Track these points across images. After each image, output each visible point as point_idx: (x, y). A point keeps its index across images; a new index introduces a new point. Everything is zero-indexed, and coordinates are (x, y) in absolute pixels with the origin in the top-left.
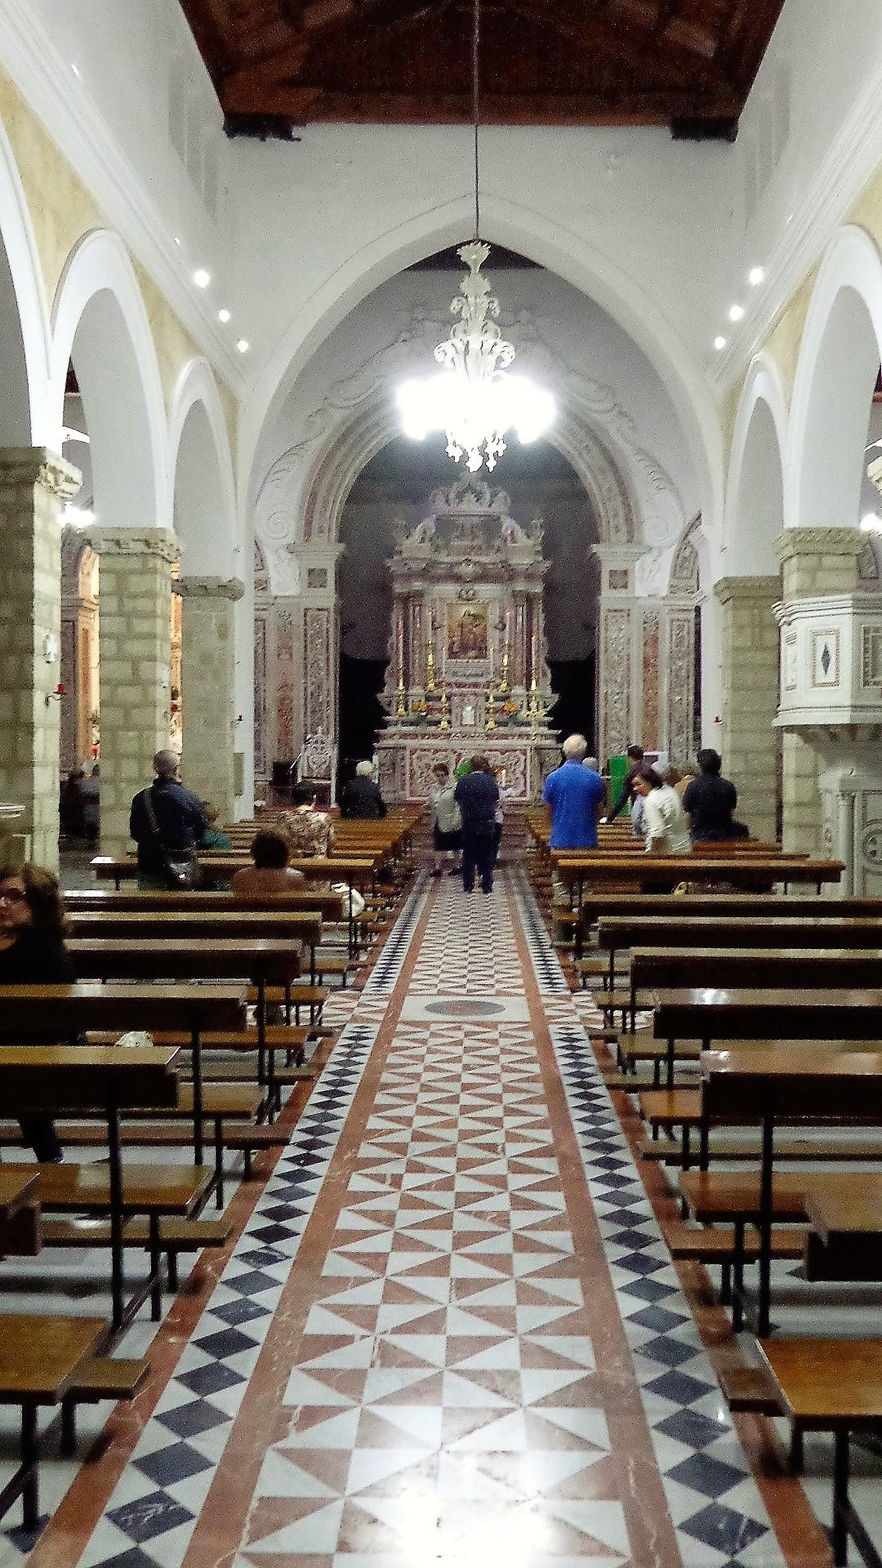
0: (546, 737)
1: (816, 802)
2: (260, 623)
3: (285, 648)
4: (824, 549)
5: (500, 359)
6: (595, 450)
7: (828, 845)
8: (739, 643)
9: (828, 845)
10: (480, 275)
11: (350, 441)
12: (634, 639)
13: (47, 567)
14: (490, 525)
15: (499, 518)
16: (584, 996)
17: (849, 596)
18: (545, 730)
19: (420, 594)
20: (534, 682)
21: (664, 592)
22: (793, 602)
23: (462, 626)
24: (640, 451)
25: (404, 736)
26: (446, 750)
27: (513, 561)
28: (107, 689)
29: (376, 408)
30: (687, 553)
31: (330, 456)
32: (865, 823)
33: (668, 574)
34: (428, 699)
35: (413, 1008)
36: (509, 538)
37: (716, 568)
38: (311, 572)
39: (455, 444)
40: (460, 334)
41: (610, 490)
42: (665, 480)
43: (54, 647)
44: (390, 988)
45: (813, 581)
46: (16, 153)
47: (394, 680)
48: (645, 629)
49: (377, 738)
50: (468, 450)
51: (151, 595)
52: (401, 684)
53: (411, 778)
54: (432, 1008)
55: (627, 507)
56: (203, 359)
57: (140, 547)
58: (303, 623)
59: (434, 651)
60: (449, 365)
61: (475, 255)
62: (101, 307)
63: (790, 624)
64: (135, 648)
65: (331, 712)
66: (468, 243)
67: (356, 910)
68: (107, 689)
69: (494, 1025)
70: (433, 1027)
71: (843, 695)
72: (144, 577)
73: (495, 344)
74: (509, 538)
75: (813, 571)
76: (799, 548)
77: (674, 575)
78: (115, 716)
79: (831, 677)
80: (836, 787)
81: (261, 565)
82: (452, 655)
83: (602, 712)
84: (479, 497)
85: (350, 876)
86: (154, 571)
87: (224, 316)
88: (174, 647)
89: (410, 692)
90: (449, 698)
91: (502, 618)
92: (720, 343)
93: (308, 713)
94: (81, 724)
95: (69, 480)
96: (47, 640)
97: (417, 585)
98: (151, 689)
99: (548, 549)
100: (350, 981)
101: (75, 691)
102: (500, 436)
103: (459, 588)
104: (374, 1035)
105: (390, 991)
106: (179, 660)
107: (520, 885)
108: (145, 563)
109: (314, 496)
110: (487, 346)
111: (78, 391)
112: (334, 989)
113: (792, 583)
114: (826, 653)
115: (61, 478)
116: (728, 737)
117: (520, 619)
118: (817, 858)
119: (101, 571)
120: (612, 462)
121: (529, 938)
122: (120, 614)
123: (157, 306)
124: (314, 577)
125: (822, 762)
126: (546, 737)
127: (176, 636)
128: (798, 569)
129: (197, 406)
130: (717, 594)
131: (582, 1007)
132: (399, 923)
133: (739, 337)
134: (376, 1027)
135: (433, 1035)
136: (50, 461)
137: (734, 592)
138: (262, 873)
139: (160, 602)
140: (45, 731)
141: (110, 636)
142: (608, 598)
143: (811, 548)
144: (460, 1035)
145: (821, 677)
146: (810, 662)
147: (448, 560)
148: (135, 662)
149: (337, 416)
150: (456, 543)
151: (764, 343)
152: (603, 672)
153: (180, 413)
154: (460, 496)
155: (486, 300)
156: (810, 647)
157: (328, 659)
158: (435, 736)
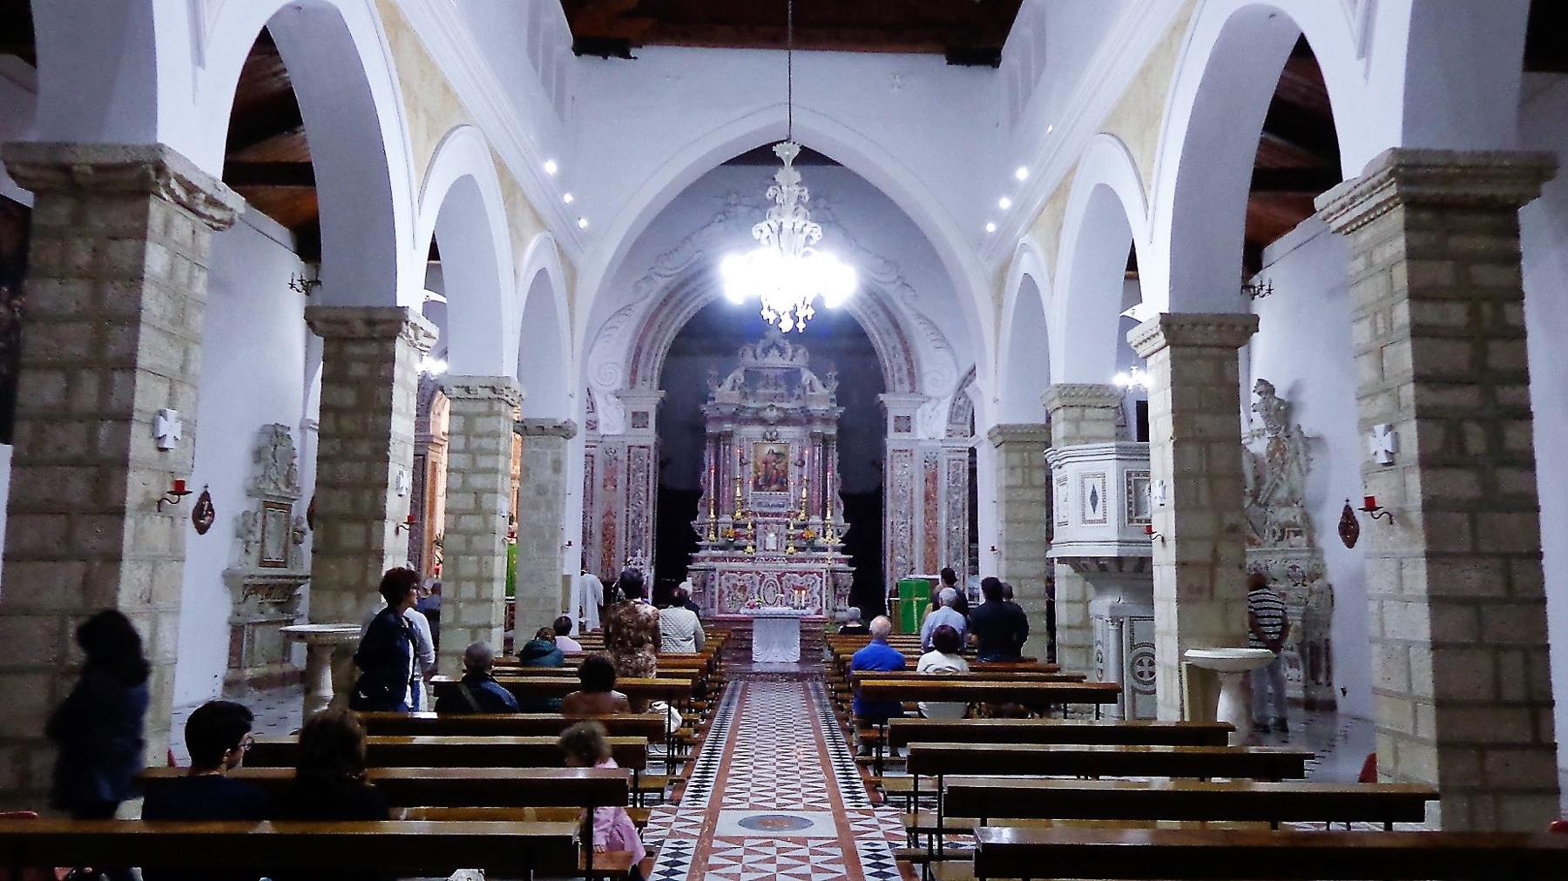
0: (840, 560)
1: (1086, 625)
2: (590, 457)
3: (610, 480)
4: (1088, 402)
5: (809, 238)
6: (882, 315)
7: (1100, 666)
8: (1012, 482)
9: (1100, 666)
10: (792, 168)
11: (671, 304)
12: (916, 475)
13: (404, 410)
14: (792, 377)
15: (799, 370)
16: (885, 810)
17: (1113, 444)
18: (838, 555)
19: (730, 435)
20: (829, 513)
21: (943, 435)
22: (1060, 447)
23: (766, 463)
24: (920, 316)
25: (714, 559)
26: (750, 572)
27: (811, 408)
28: (452, 518)
29: (700, 273)
30: (961, 402)
31: (654, 316)
32: (1133, 647)
33: (946, 420)
34: (735, 526)
35: (728, 824)
36: (808, 389)
37: (990, 417)
38: (635, 414)
39: (769, 309)
40: (774, 216)
41: (894, 348)
42: (943, 341)
43: (406, 482)
44: (704, 803)
45: (1078, 428)
46: (397, 62)
47: (706, 510)
48: (925, 467)
49: (691, 560)
50: (781, 314)
51: (495, 435)
52: (712, 513)
53: (719, 597)
54: (743, 823)
55: (909, 361)
56: (549, 235)
57: (487, 393)
58: (626, 459)
59: (742, 483)
60: (766, 242)
61: (787, 152)
62: (463, 189)
63: (1060, 467)
64: (478, 481)
65: (649, 537)
66: (782, 142)
67: (674, 726)
68: (452, 518)
69: (803, 841)
70: (747, 843)
71: (1110, 531)
72: (489, 419)
73: (806, 225)
74: (808, 389)
75: (1077, 422)
76: (1065, 401)
77: (950, 421)
78: (456, 542)
79: (1099, 515)
80: (1106, 614)
81: (592, 407)
82: (757, 487)
83: (889, 539)
84: (782, 352)
85: (668, 694)
86: (499, 414)
87: (568, 198)
88: (513, 478)
89: (721, 520)
90: (754, 526)
91: (802, 455)
92: (991, 227)
93: (630, 538)
94: (426, 546)
95: (428, 335)
96: (400, 474)
97: (728, 427)
98: (492, 518)
99: (841, 397)
100: (668, 794)
101: (422, 517)
102: (809, 301)
103: (765, 430)
104: (691, 851)
105: (705, 805)
106: (516, 489)
107: (819, 697)
108: (491, 407)
109: (639, 350)
110: (798, 227)
111: (439, 259)
112: (653, 802)
113: (1059, 430)
114: (1094, 493)
115: (421, 333)
116: (1003, 564)
117: (817, 457)
118: (1093, 680)
119: (451, 413)
120: (896, 326)
121: (830, 750)
122: (467, 450)
123: (510, 188)
124: (638, 419)
125: (1091, 590)
126: (840, 560)
127: (516, 470)
128: (1064, 420)
129: (542, 273)
130: (990, 438)
131: (886, 822)
132: (711, 736)
133: (1008, 224)
134: (693, 843)
135: (748, 851)
136: (412, 319)
137: (1008, 438)
138: (589, 697)
139: (503, 441)
140: (394, 557)
141: (458, 471)
142: (893, 440)
143: (1072, 401)
144: (772, 851)
145: (1090, 515)
146: (1079, 501)
147: (755, 405)
148: (477, 493)
149: (661, 282)
150: (761, 391)
151: (1031, 227)
152: (890, 505)
153: (527, 277)
154: (766, 351)
155: (797, 189)
156: (1079, 489)
157: (648, 490)
158: (742, 559)
